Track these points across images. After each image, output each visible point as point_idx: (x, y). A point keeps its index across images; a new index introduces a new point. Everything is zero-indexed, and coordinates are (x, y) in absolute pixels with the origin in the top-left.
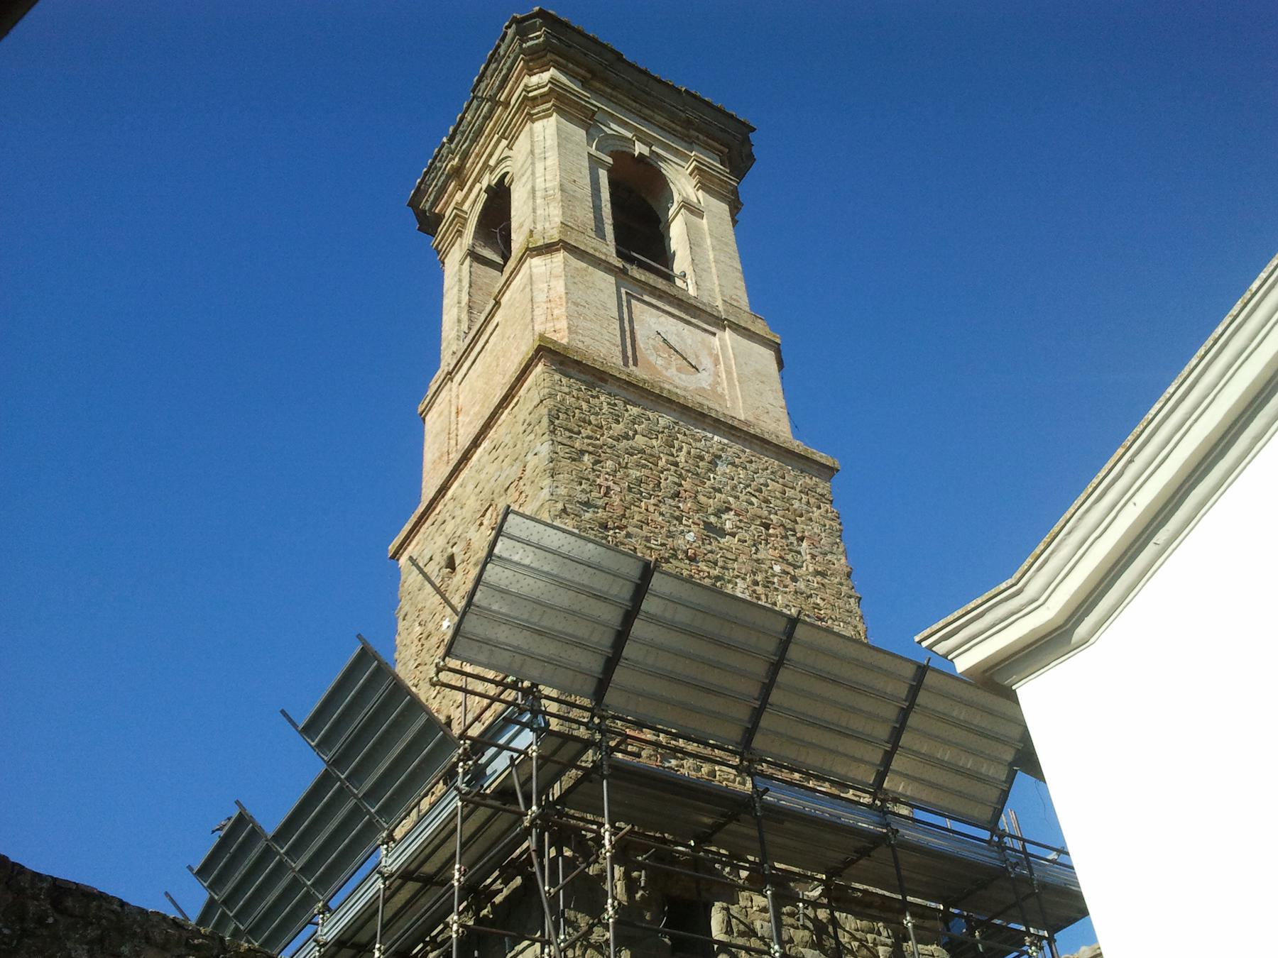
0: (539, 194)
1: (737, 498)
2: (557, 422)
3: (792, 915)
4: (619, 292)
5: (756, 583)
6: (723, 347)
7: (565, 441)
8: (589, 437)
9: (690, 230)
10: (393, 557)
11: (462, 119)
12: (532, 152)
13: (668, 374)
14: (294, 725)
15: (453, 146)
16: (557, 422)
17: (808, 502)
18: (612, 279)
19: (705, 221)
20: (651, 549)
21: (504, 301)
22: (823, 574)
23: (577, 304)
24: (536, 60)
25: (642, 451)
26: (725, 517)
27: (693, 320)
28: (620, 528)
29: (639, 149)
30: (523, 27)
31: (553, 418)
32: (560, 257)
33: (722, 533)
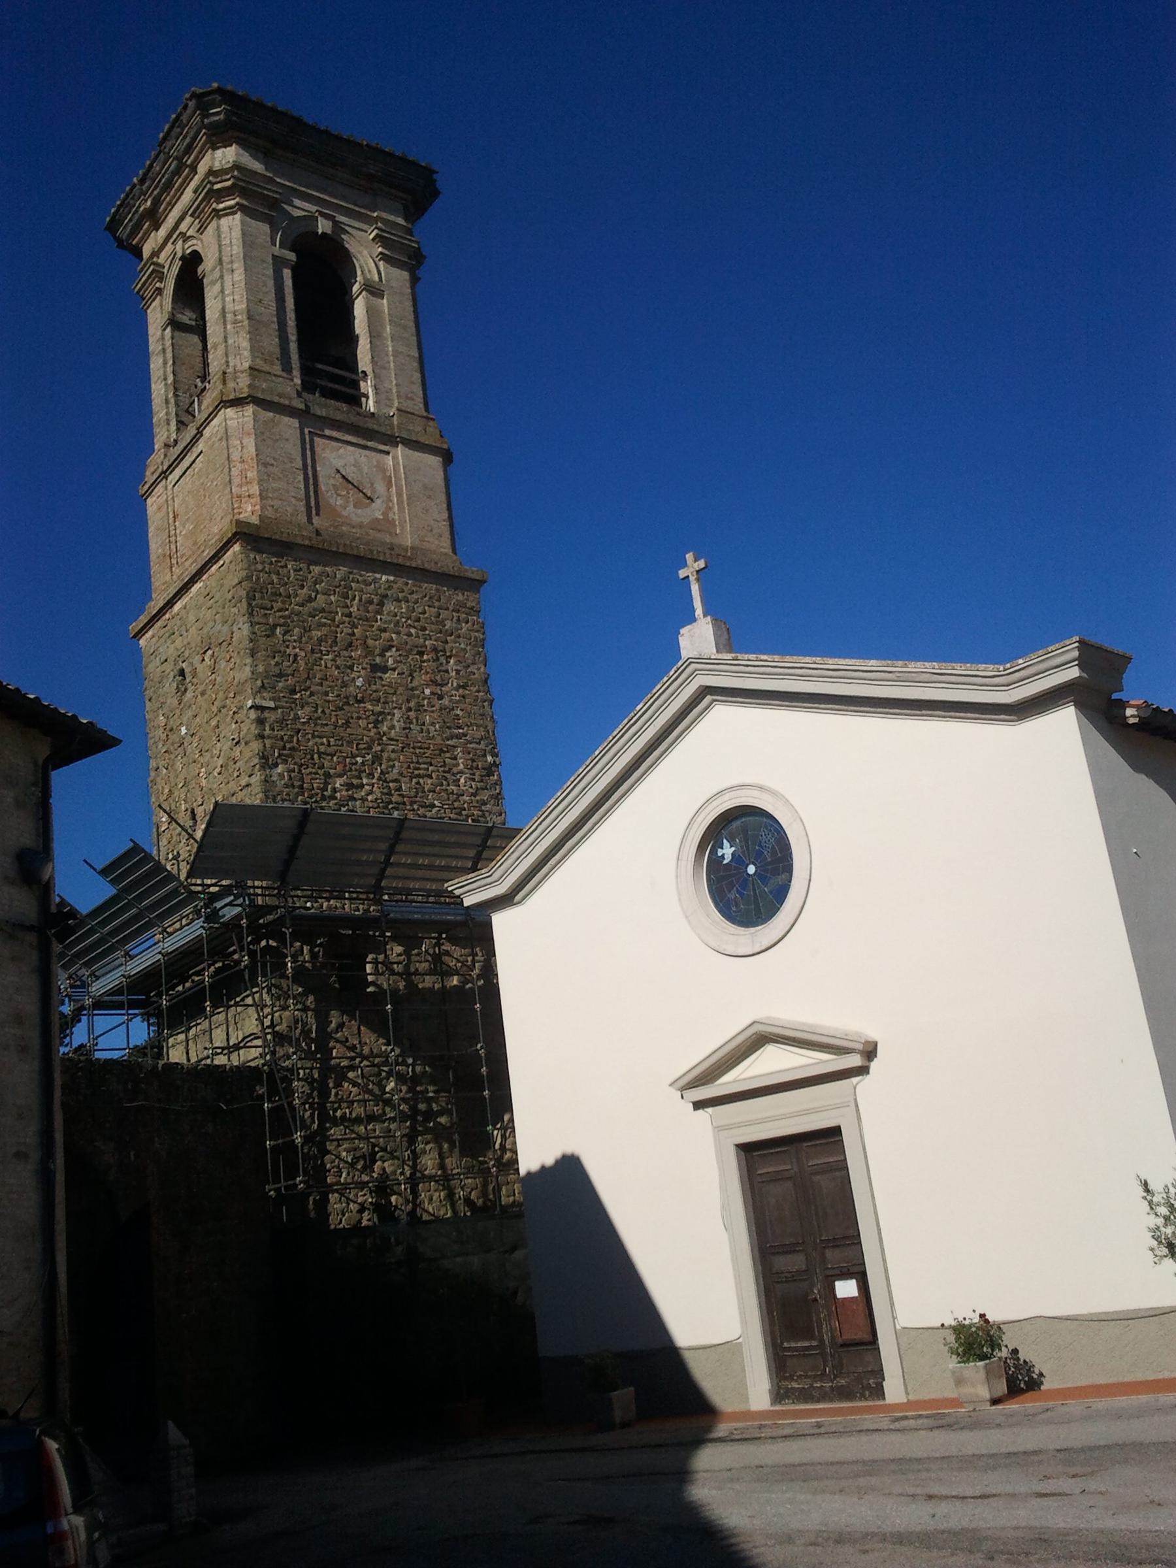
0: (229, 316)
1: (398, 633)
2: (254, 603)
3: (418, 954)
4: (302, 434)
5: (410, 709)
6: (396, 465)
7: (262, 620)
8: (279, 611)
9: (371, 312)
10: (134, 637)
11: (151, 166)
12: (220, 260)
13: (345, 513)
14: (95, 869)
15: (144, 187)
16: (254, 603)
17: (458, 620)
18: (295, 423)
19: (385, 301)
20: (329, 702)
21: (207, 432)
22: (464, 687)
23: (266, 465)
24: (218, 137)
25: (323, 610)
26: (388, 654)
27: (369, 444)
28: (305, 690)
29: (323, 226)
30: (203, 103)
31: (251, 598)
32: (250, 410)
33: (385, 669)
